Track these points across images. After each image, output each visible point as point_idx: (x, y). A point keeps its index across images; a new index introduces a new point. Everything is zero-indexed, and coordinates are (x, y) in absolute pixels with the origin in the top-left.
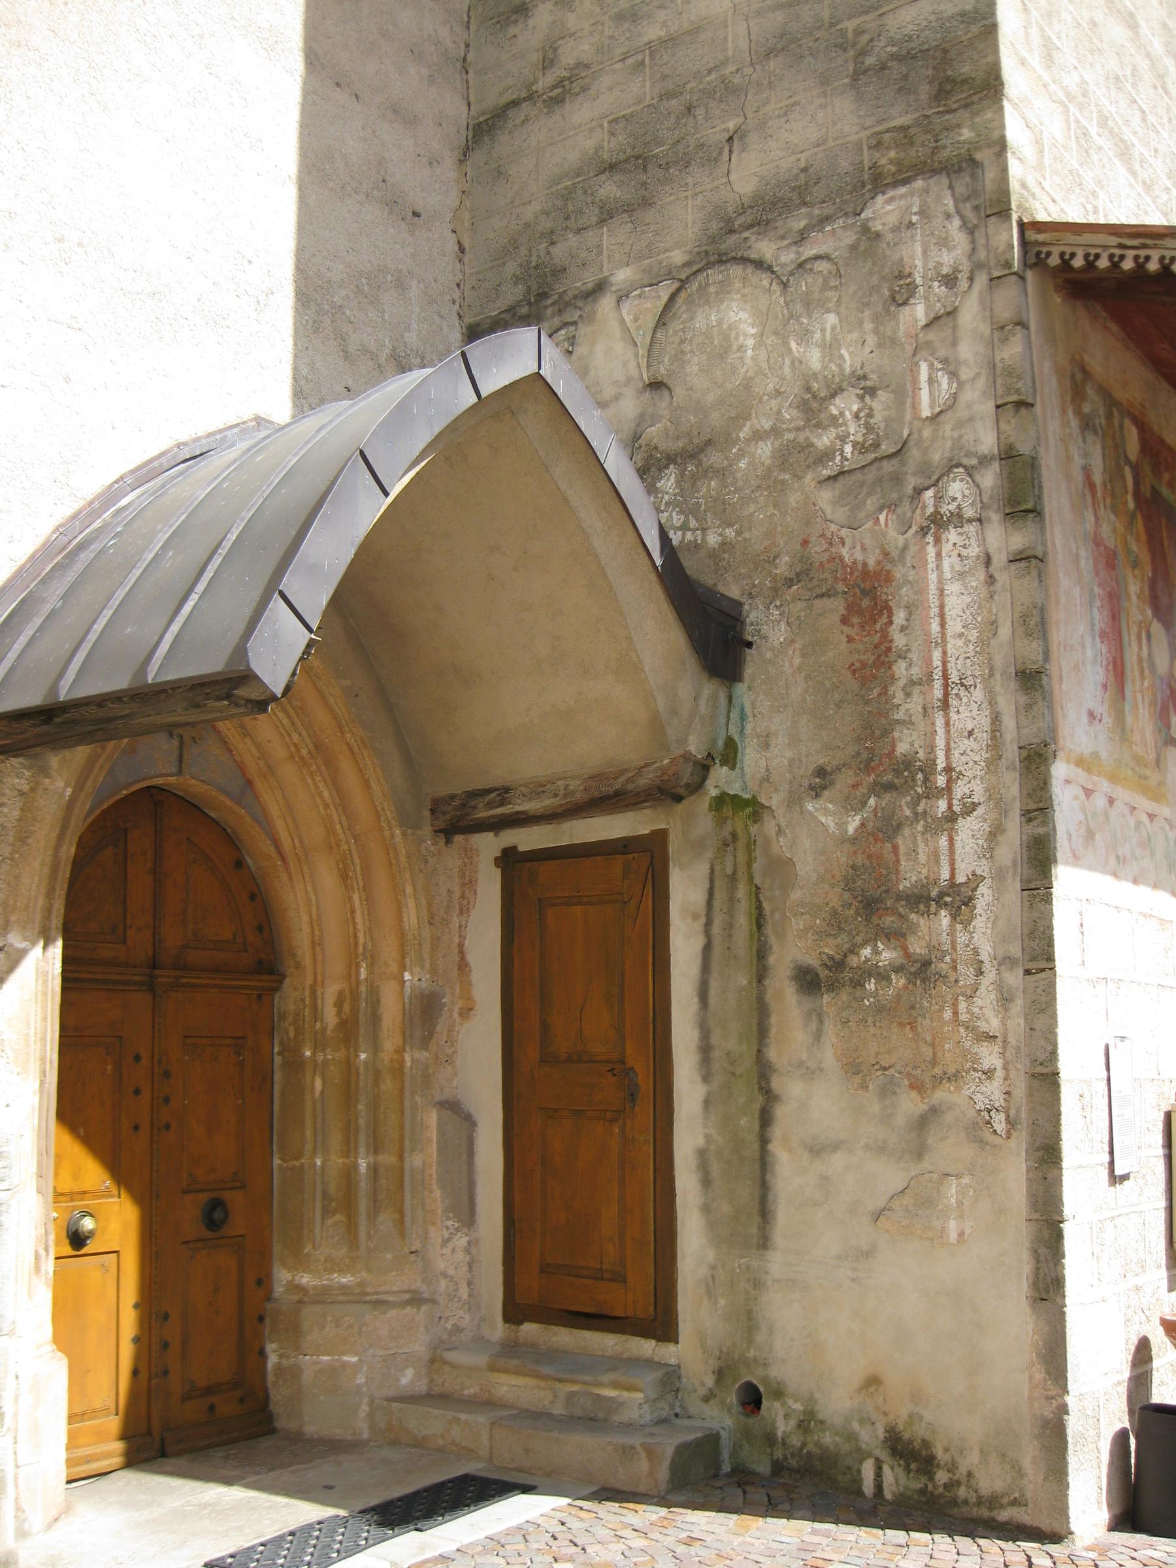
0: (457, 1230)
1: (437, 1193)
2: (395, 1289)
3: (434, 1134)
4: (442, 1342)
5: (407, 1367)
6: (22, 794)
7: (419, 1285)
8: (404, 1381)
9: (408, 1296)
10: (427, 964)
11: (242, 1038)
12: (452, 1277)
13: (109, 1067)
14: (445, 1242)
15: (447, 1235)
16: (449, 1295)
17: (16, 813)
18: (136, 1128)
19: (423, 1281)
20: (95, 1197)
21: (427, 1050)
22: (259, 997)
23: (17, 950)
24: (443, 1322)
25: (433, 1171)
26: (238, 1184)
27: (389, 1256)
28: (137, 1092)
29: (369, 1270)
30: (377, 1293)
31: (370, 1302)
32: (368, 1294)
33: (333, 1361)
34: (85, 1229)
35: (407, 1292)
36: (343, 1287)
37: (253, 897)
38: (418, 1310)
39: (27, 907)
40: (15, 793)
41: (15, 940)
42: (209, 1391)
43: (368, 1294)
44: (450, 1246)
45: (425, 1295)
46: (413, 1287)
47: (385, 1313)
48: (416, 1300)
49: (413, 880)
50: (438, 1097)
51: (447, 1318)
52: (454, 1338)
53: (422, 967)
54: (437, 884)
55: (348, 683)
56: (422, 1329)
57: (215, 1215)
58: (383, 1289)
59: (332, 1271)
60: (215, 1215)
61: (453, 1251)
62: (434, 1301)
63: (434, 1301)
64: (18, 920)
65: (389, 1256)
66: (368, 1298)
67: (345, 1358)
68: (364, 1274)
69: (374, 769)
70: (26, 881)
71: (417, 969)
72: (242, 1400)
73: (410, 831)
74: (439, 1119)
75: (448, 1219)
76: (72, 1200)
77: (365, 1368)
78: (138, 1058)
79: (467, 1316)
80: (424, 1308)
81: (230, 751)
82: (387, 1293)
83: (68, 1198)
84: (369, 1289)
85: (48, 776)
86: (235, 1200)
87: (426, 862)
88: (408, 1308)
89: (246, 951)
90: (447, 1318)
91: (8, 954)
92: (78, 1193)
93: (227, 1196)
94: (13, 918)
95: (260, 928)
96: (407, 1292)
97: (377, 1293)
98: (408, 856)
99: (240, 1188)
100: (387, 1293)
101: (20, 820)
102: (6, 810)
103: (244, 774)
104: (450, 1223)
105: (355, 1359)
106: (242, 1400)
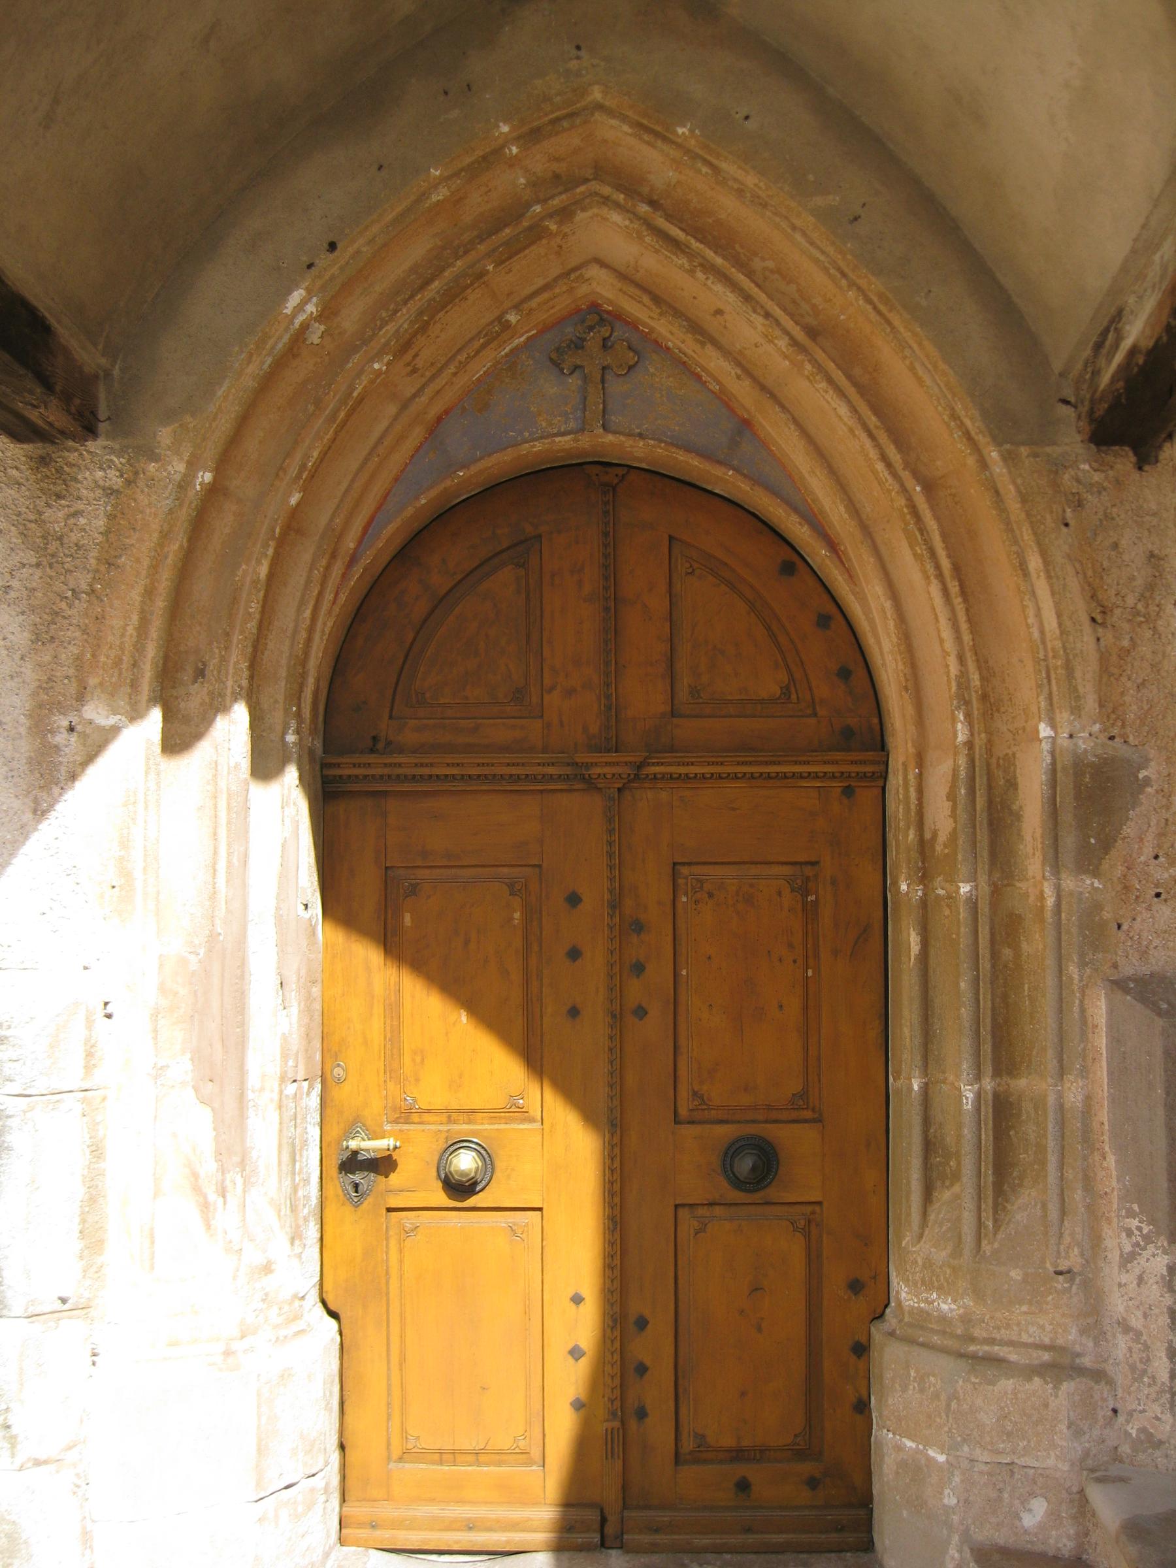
0: (1147, 1239)
1: (1111, 1160)
2: (1025, 1338)
3: (1101, 1041)
4: (1117, 1458)
5: (1032, 1495)
6: (110, 492)
7: (1071, 1336)
8: (1029, 1521)
9: (1046, 1357)
10: (1090, 703)
11: (813, 864)
12: (1139, 1334)
13: (517, 915)
14: (1127, 1260)
15: (1128, 1248)
16: (1133, 1368)
17: (101, 523)
18: (574, 1012)
19: (1083, 1332)
20: (493, 1121)
21: (1096, 874)
22: (848, 791)
23: (102, 729)
24: (1121, 1419)
25: (1103, 1115)
26: (808, 1114)
27: (1016, 1274)
28: (574, 954)
29: (978, 1294)
30: (992, 1341)
31: (974, 1357)
32: (972, 1340)
33: (917, 1451)
34: (463, 1174)
35: (1046, 1348)
36: (943, 1319)
37: (824, 621)
38: (1056, 1387)
39: (118, 662)
40: (99, 492)
41: (97, 713)
42: (738, 1455)
43: (972, 1340)
44: (1136, 1268)
45: (1087, 1361)
46: (1060, 1342)
47: (992, 1383)
48: (1060, 1366)
49: (1039, 544)
50: (1130, 967)
51: (1130, 1414)
52: (1141, 1457)
53: (1076, 710)
54: (1116, 546)
55: (834, 200)
56: (1063, 1427)
57: (755, 1166)
58: (1004, 1334)
59: (930, 1287)
60: (755, 1166)
61: (1140, 1280)
62: (1098, 1375)
63: (1098, 1375)
64: (101, 684)
65: (1016, 1274)
66: (972, 1348)
67: (931, 1453)
68: (968, 1301)
69: (920, 344)
70: (117, 623)
71: (1063, 716)
72: (813, 1483)
73: (1024, 451)
74: (1111, 1012)
75: (1131, 1214)
76: (450, 1121)
77: (957, 1479)
78: (574, 900)
79: (1167, 1417)
80: (1067, 1387)
81: (698, 377)
82: (1011, 1343)
83: (444, 1117)
84: (977, 1333)
85: (154, 457)
86: (798, 1142)
87: (1080, 504)
88: (1037, 1380)
89: (815, 715)
90: (1130, 1414)
91: (84, 736)
92: (460, 1111)
93: (782, 1135)
94: (93, 681)
95: (845, 674)
96: (1046, 1348)
97: (992, 1341)
98: (1024, 499)
99: (814, 1121)
100: (1011, 1343)
101: (107, 533)
102: (82, 521)
103: (732, 410)
104: (1134, 1223)
105: (942, 1458)
106: (813, 1483)
